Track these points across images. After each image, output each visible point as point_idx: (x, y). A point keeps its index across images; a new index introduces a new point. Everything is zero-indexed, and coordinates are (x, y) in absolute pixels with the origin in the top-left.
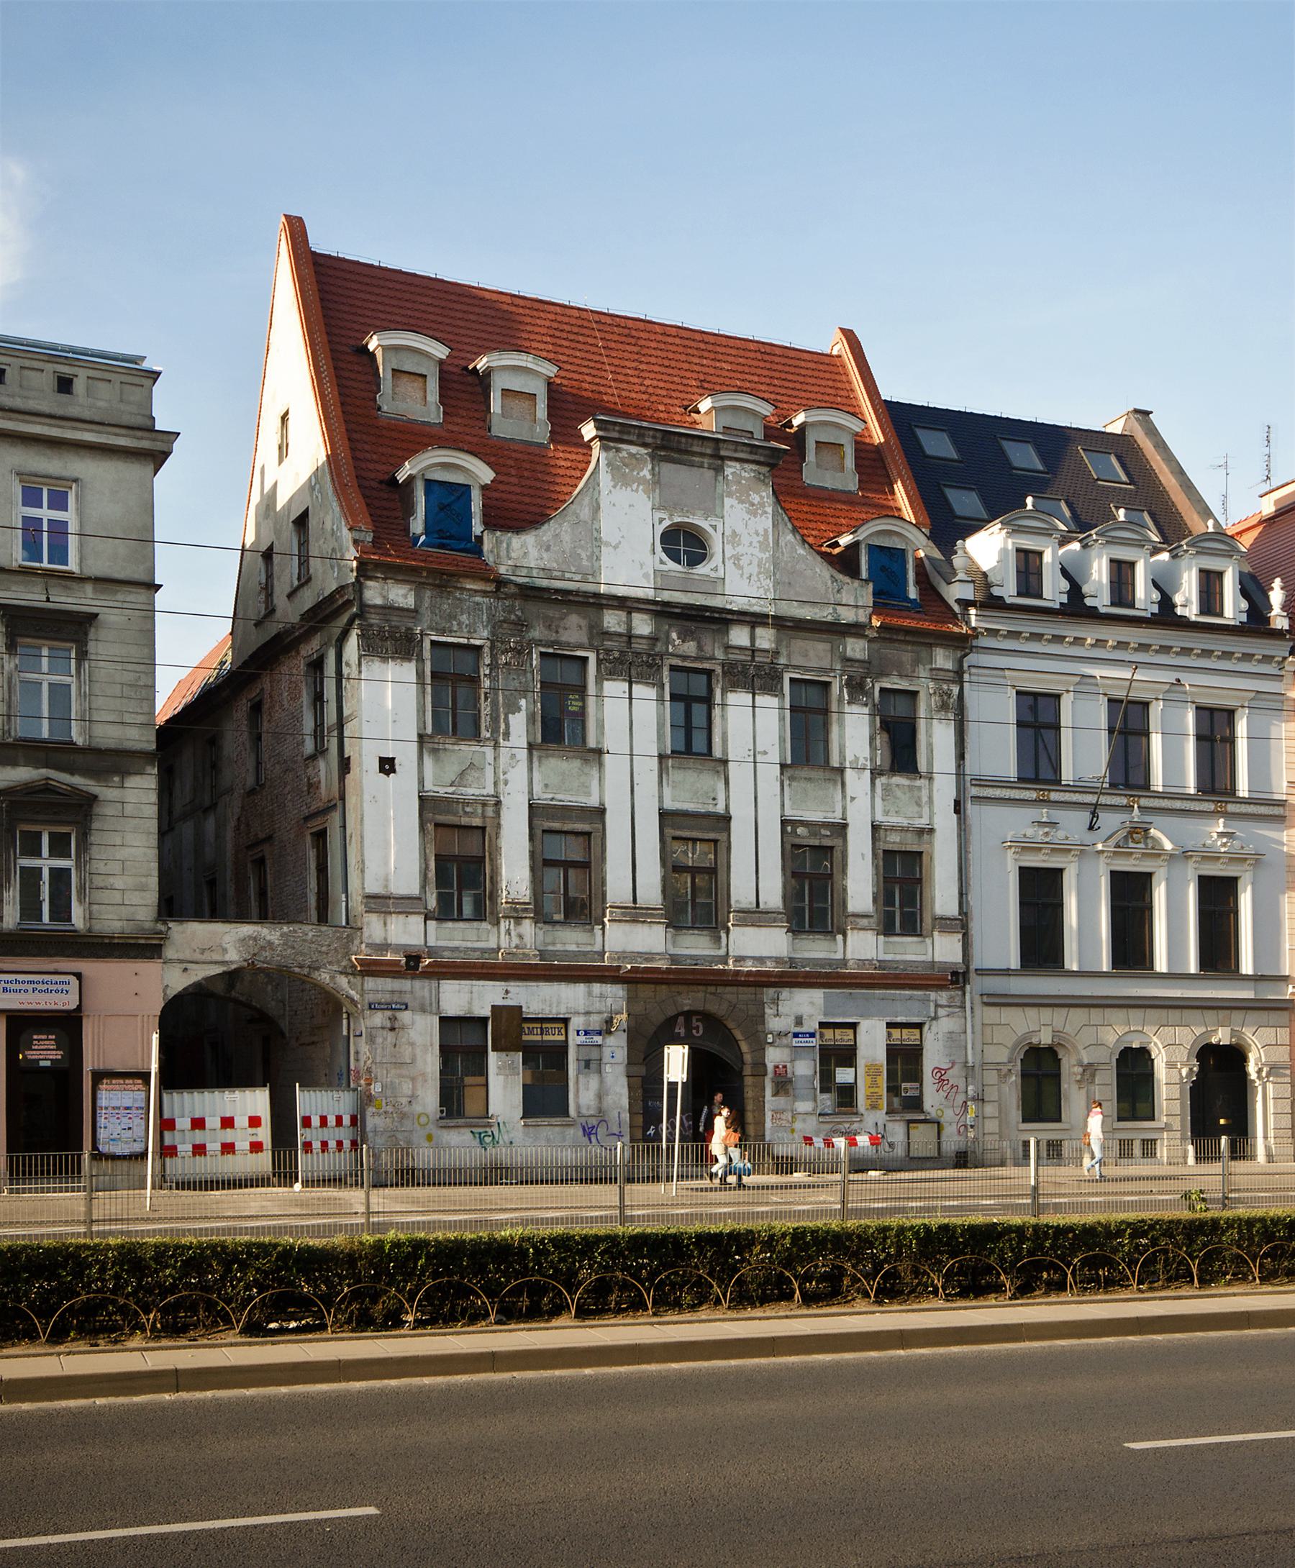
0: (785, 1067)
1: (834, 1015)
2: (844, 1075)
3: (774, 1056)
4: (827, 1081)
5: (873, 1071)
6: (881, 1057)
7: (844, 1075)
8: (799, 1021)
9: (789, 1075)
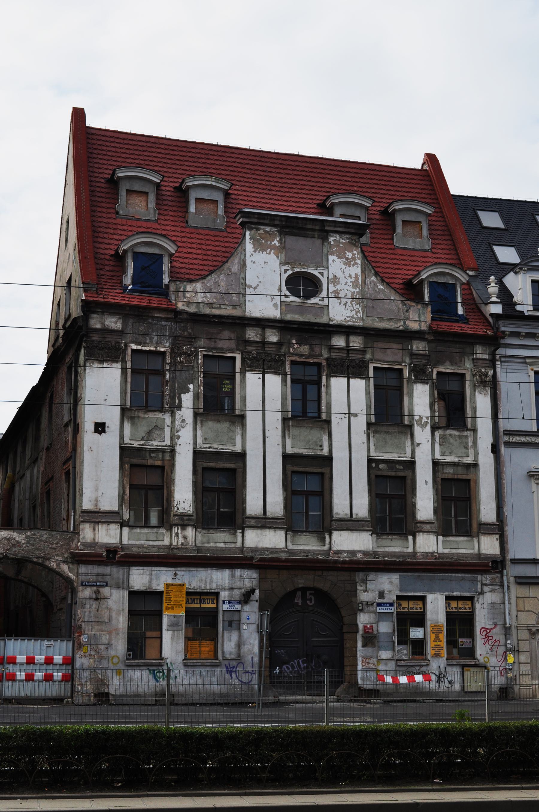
0: (372, 626)
1: (407, 591)
2: (416, 633)
3: (363, 619)
4: (403, 637)
5: (437, 630)
6: (442, 619)
7: (416, 633)
8: (382, 594)
9: (375, 632)
